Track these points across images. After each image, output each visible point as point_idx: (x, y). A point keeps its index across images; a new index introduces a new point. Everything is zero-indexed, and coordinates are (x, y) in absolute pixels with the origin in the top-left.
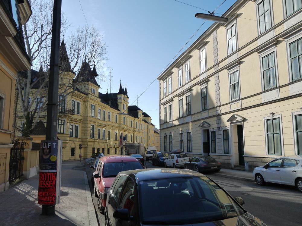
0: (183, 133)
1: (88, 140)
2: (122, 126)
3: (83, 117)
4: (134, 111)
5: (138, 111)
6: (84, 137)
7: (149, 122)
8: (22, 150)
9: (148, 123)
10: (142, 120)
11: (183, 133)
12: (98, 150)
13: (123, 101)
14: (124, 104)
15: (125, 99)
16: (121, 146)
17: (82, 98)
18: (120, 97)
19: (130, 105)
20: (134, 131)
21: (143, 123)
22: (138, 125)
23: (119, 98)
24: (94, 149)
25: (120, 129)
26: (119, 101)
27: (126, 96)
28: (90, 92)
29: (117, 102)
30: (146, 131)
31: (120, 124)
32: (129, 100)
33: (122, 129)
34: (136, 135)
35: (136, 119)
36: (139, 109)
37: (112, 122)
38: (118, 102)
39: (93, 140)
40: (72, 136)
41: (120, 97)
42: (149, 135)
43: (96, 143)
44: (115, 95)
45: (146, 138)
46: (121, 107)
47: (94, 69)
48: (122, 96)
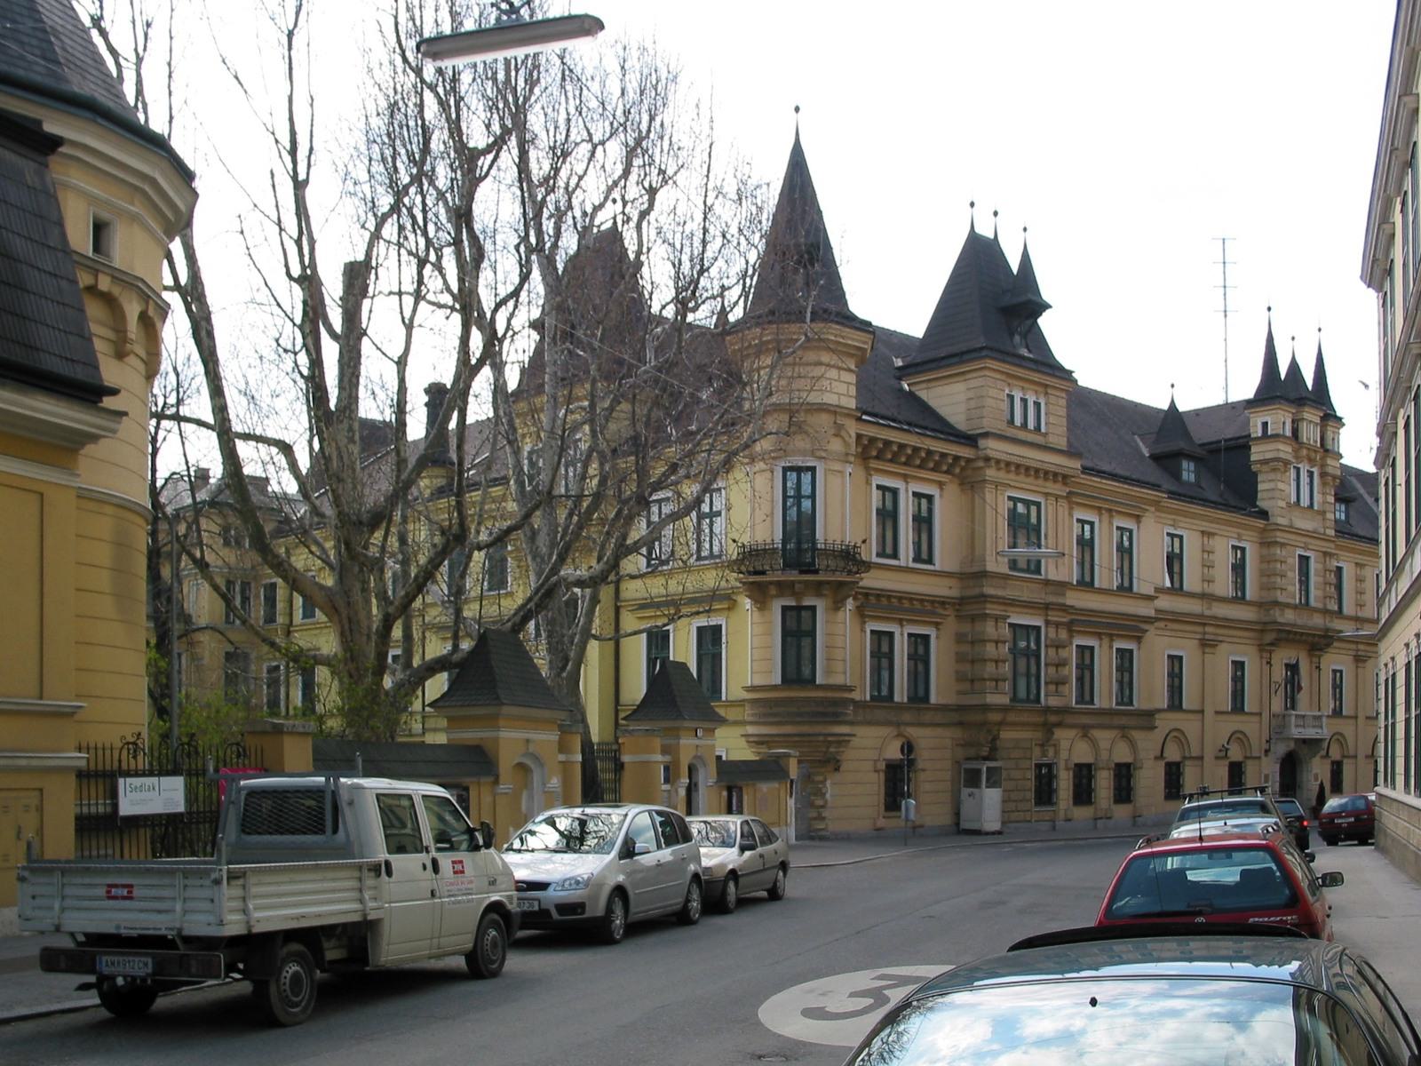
3: (961, 576)
15: (1310, 434)
16: (1281, 749)
18: (1265, 425)
26: (1257, 452)
27: (1312, 415)
29: (1249, 456)
38: (1253, 458)
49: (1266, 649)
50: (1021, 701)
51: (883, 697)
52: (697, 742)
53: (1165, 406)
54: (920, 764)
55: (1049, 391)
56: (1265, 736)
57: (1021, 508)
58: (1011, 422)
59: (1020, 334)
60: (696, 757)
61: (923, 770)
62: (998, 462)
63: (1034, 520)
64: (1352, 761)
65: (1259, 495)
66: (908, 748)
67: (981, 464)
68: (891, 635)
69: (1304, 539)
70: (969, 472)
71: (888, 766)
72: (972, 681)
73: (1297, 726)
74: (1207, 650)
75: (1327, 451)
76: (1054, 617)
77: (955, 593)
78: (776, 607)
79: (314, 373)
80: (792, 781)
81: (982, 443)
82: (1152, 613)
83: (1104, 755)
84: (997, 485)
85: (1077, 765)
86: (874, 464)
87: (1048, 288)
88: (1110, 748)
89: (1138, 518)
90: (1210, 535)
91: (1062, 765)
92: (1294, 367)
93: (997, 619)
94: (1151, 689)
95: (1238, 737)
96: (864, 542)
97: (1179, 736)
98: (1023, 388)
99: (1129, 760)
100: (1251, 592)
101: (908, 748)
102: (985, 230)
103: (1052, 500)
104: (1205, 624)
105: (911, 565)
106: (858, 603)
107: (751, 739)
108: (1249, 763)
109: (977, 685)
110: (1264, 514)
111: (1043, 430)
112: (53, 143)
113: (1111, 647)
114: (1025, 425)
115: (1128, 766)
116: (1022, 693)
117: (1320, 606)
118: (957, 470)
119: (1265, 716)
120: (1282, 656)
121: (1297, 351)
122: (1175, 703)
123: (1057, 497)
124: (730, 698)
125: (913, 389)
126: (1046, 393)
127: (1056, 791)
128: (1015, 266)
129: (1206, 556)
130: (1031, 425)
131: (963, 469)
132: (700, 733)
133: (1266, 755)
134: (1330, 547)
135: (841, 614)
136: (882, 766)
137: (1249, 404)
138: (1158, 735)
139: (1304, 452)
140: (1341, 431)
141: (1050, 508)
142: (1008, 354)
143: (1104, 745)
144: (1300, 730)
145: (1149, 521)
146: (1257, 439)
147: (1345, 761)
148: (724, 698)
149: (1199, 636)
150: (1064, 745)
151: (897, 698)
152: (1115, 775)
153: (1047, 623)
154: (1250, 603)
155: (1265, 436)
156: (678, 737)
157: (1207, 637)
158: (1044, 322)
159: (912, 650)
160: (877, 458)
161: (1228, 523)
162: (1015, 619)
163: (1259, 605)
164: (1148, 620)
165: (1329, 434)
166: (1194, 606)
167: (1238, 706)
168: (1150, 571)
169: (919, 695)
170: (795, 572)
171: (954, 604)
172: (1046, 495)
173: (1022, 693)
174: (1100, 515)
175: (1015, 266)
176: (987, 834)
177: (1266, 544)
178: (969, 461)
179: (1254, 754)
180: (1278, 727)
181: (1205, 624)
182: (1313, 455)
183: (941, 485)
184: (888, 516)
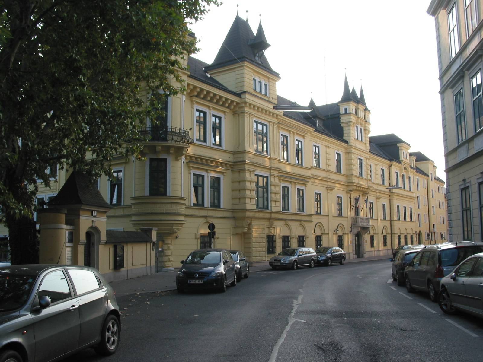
0: (468, 187)
1: (248, 214)
2: (355, 180)
3: (234, 153)
4: (388, 147)
5: (398, 145)
6: (237, 207)
7: (430, 171)
8: (213, 185)
9: (429, 176)
10: (411, 167)
11: (468, 187)
12: (286, 239)
13: (353, 118)
14: (359, 127)
15: (361, 114)
16: (355, 231)
17: (227, 105)
18: (346, 110)
19: (371, 135)
20: (391, 195)
21: (413, 176)
22: (407, 181)
23: (342, 111)
24: (271, 239)
25: (350, 188)
26: (343, 119)
27: (361, 107)
28: (367, 193)
29: (339, 121)
30: (422, 193)
31: (349, 176)
32: (372, 118)
33: (355, 188)
34: (396, 202)
35: (394, 163)
36: (401, 141)
37: (327, 171)
38: (341, 121)
39: (267, 215)
40: (203, 205)
41: (346, 110)
42: (432, 204)
43: (276, 223)
44: (335, 107)
45: (423, 211)
46: (351, 133)
47: (260, 30)
48: (351, 107)
49: (349, 192)
50: (260, 208)
51: (200, 204)
52: (94, 219)
53: (306, 104)
54: (216, 236)
55: (270, 80)
56: (350, 226)
57: (260, 127)
58: (255, 90)
59: (258, 56)
60: (92, 227)
61: (218, 238)
62: (250, 105)
63: (265, 131)
65: (344, 135)
66: (212, 227)
67: (243, 105)
68: (203, 176)
69: (360, 153)
70: (237, 109)
71: (202, 236)
72: (240, 199)
73: (361, 222)
74: (329, 191)
75: (366, 121)
76: (273, 173)
77: (231, 160)
78: (146, 159)
80: (154, 243)
81: (243, 96)
82: (310, 175)
84: (250, 114)
85: (283, 236)
86: (195, 99)
87: (269, 38)
88: (296, 231)
89: (304, 137)
90: (329, 147)
92: (354, 90)
93: (250, 171)
94: (311, 207)
95: (340, 225)
96: (191, 129)
97: (319, 225)
98: (260, 77)
99: (289, 235)
100: (343, 171)
101: (212, 227)
102: (243, 17)
103: (271, 124)
104: (328, 181)
105: (212, 146)
106: (187, 161)
107: (133, 223)
108: (323, 236)
109: (242, 201)
110: (346, 142)
111: (268, 95)
113: (295, 188)
114: (261, 92)
115: (303, 237)
116: (261, 205)
117: (366, 177)
118: (232, 107)
119: (349, 218)
120: (354, 195)
121: (355, 86)
123: (274, 123)
124: (126, 204)
125: (212, 76)
126: (269, 81)
127: (275, 247)
128: (255, 32)
129: (327, 156)
130: (263, 92)
131: (235, 106)
132: (95, 214)
133: (350, 233)
134: (368, 156)
135: (179, 163)
137: (340, 102)
138: (313, 224)
139: (359, 121)
140: (370, 115)
141: (271, 127)
142: (254, 61)
144: (362, 223)
145: (308, 137)
146: (343, 114)
147: (375, 236)
148: (122, 204)
149: (326, 186)
151: (206, 205)
152: (298, 241)
153: (271, 175)
154: (343, 175)
157: (329, 186)
158: (267, 53)
159: (213, 201)
160: (197, 96)
161: (335, 144)
162: (258, 173)
163: (347, 176)
164: (310, 178)
165: (367, 116)
166: (323, 174)
167: (340, 215)
168: (309, 160)
169: (216, 205)
170: (140, 111)
171: (230, 165)
172: (269, 122)
173: (261, 205)
174: (290, 133)
175: (255, 32)
176: (202, 264)
177: (348, 153)
178: (238, 103)
179: (347, 233)
180: (354, 221)
181: (328, 181)
182: (362, 122)
183: (224, 112)
184: (202, 123)
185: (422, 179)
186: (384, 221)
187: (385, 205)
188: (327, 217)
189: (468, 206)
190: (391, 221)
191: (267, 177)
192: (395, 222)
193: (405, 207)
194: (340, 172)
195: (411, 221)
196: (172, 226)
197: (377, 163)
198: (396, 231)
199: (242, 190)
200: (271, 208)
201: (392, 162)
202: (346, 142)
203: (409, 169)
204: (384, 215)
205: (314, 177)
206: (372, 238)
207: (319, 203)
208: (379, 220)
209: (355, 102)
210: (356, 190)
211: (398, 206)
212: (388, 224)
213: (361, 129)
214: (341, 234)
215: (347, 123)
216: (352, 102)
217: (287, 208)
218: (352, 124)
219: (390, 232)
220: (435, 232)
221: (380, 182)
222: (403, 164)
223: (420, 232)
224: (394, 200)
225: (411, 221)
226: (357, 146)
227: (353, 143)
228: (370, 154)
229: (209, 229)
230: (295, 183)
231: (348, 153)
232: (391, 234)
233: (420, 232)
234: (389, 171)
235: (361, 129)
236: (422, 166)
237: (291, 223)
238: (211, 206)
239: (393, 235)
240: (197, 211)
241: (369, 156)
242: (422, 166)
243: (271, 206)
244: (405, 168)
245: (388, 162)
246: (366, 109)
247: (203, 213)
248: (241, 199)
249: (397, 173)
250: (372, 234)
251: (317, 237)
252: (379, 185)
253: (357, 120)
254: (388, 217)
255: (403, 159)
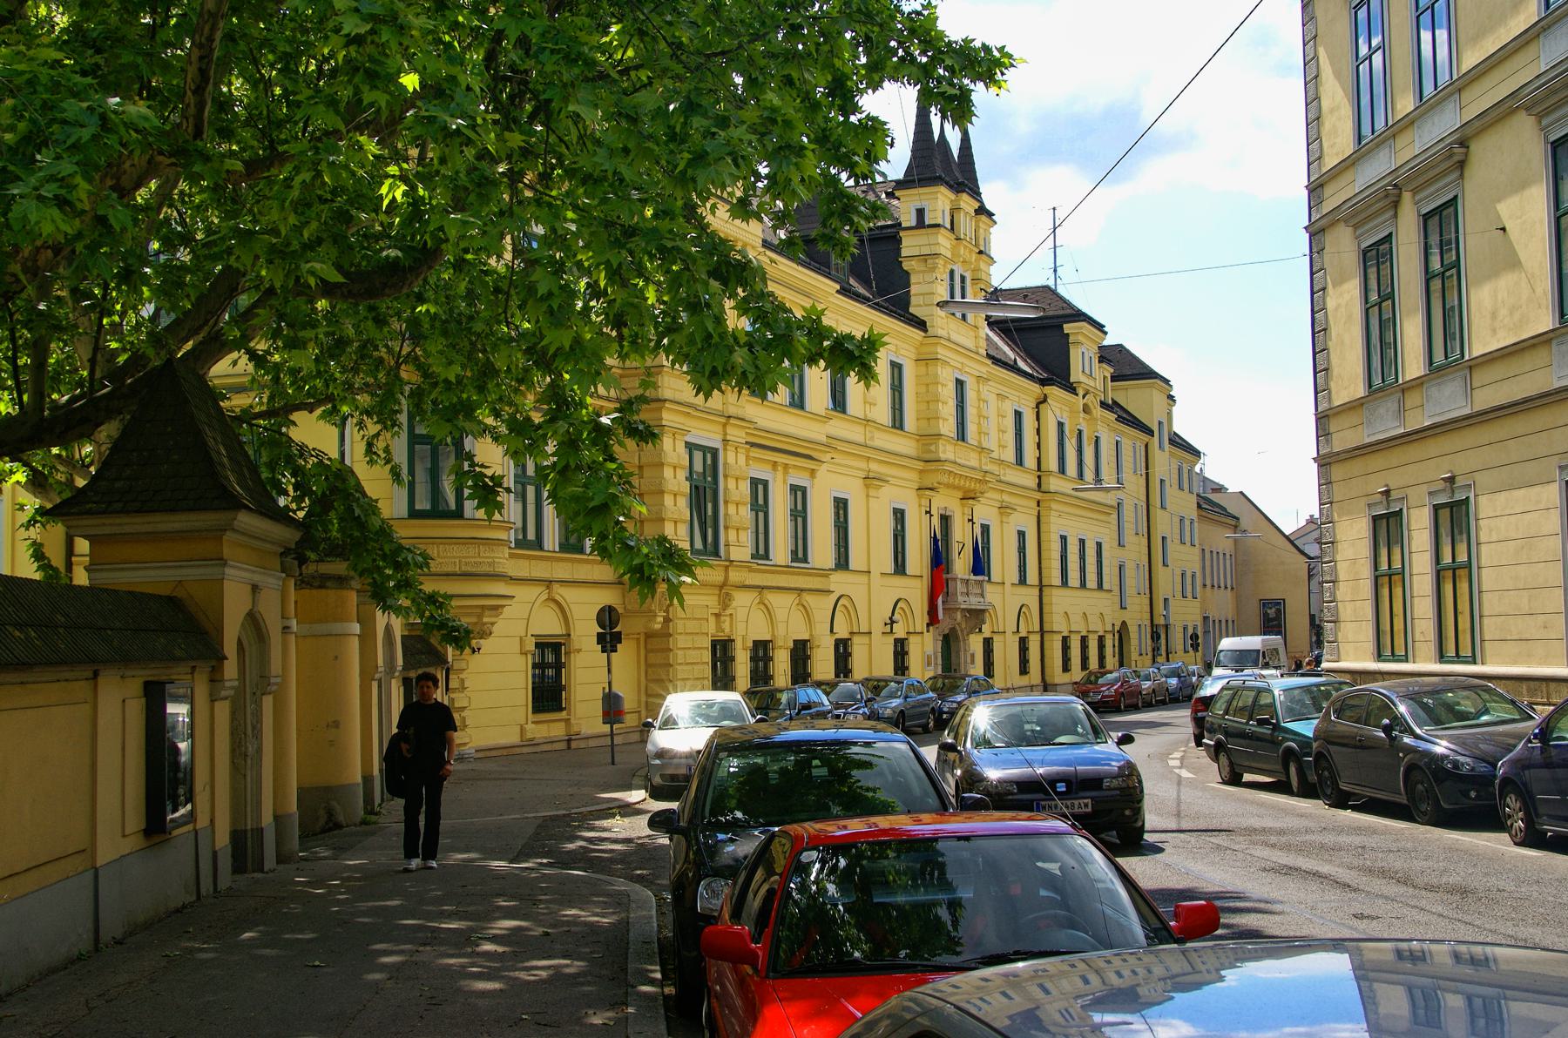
15: (966, 224)
18: (920, 213)
26: (911, 245)
29: (899, 250)
31: (929, 438)
35: (1054, 391)
38: (904, 253)
40: (538, 544)
41: (920, 213)
45: (1135, 550)
46: (926, 291)
48: (939, 201)
64: (865, 639)
65: (914, 300)
79: (33, 469)
83: (781, 630)
91: (738, 644)
99: (768, 638)
108: (856, 640)
110: (921, 324)
112: (276, 818)
122: (842, 563)
136: (530, 645)
138: (833, 598)
143: (780, 615)
150: (741, 614)
155: (921, 223)
156: (660, 410)
177: (926, 360)
185: (1131, 440)
186: (899, 581)
187: (902, 512)
188: (864, 578)
189: (1397, 565)
190: (1041, 587)
191: (714, 452)
192: (1055, 592)
193: (1082, 542)
194: (901, 428)
195: (1100, 586)
196: (480, 616)
197: (1004, 390)
198: (1058, 623)
199: (652, 493)
200: (728, 552)
201: (1048, 390)
202: (921, 324)
203: (1098, 412)
204: (838, 546)
205: (831, 444)
206: (988, 644)
207: (761, 515)
208: (1008, 585)
209: (951, 187)
210: (948, 486)
211: (1064, 539)
212: (1030, 596)
213: (963, 279)
214: (845, 635)
215: (924, 258)
216: (943, 189)
217: (800, 555)
218: (940, 262)
219: (1037, 628)
220: (1167, 627)
221: (1010, 455)
222: (1081, 392)
223: (1124, 623)
224: (1053, 519)
225: (1100, 586)
226: (954, 337)
227: (941, 322)
228: (989, 362)
229: (601, 625)
230: (786, 466)
231: (926, 360)
232: (1042, 632)
233: (1124, 623)
234: (1038, 419)
235: (963, 279)
236: (1133, 397)
237: (773, 599)
238: (560, 545)
239: (1046, 637)
240: (526, 563)
241: (984, 369)
242: (1133, 397)
243: (727, 545)
244: (1086, 409)
245: (1035, 388)
246: (982, 210)
247: (540, 570)
248: (646, 524)
249: (1061, 425)
250: (987, 634)
251: (838, 643)
252: (879, 427)
253: (954, 249)
254: (1032, 577)
255: (1083, 379)
